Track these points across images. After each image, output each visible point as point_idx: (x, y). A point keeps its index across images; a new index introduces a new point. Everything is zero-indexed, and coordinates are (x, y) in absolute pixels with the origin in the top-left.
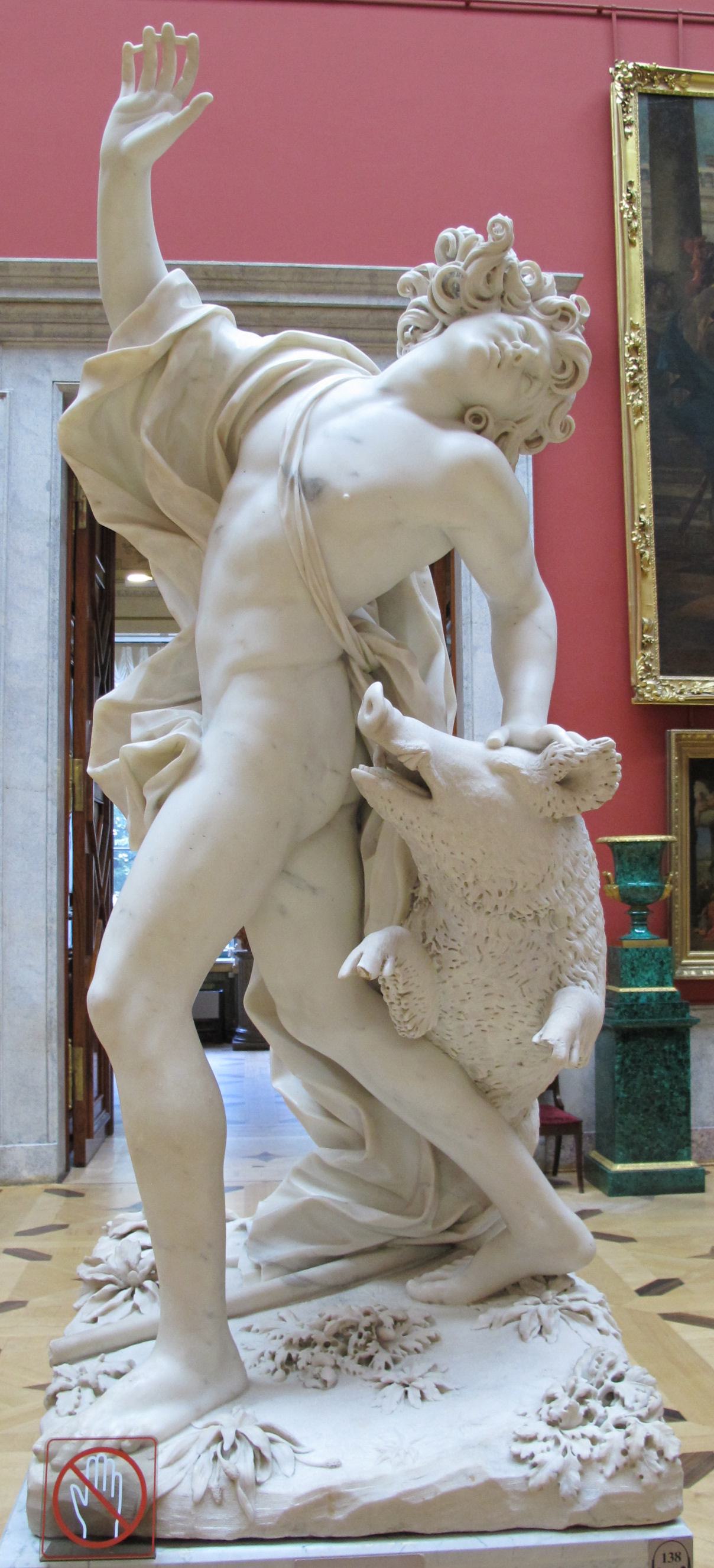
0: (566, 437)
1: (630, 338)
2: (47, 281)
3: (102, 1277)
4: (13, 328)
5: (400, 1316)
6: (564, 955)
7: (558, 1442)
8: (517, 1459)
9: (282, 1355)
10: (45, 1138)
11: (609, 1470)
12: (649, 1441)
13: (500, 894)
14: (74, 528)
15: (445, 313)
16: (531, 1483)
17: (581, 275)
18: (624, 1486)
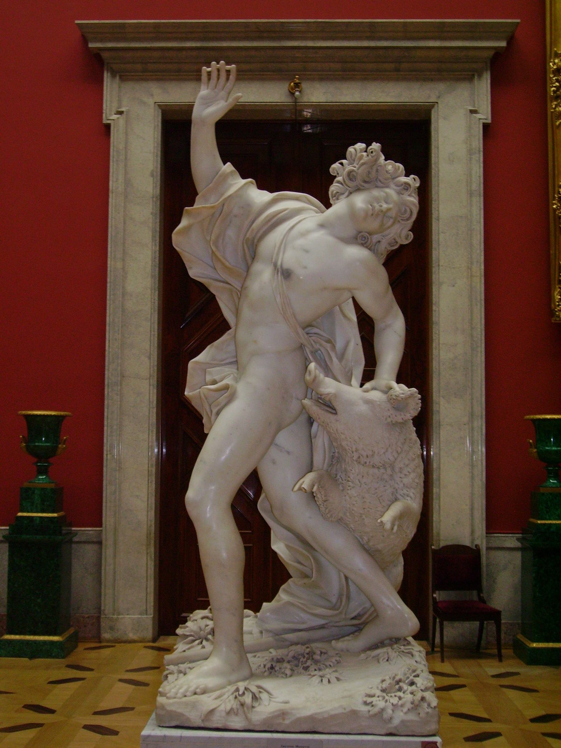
1: (554, 64)
3: (188, 634)
5: (323, 651)
7: (384, 698)
8: (365, 703)
9: (269, 665)
10: (145, 612)
11: (405, 710)
12: (423, 699)
13: (367, 456)
15: (350, 187)
16: (371, 713)
17: (518, 21)
18: (412, 717)
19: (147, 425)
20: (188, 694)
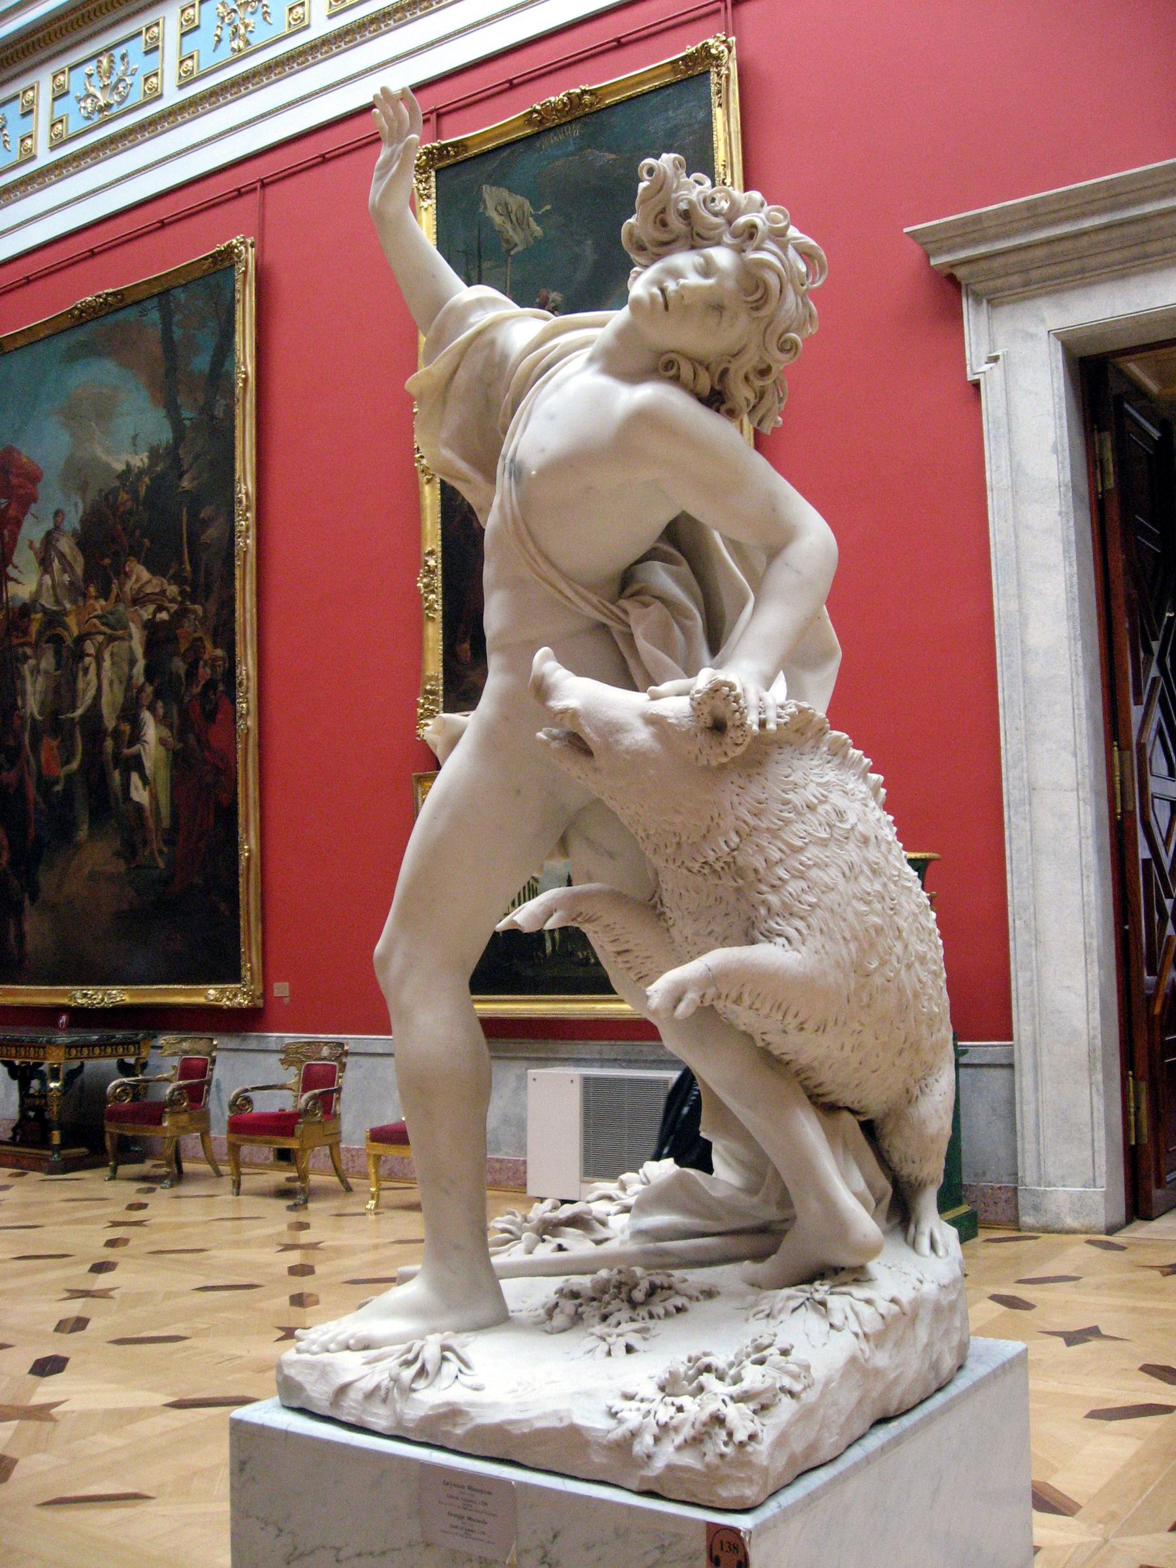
0: (791, 359)
2: (1025, 223)
4: (999, 282)
6: (757, 910)
11: (679, 1439)
14: (1100, 490)
18: (688, 1459)
19: (1077, 868)
20: (332, 1346)
